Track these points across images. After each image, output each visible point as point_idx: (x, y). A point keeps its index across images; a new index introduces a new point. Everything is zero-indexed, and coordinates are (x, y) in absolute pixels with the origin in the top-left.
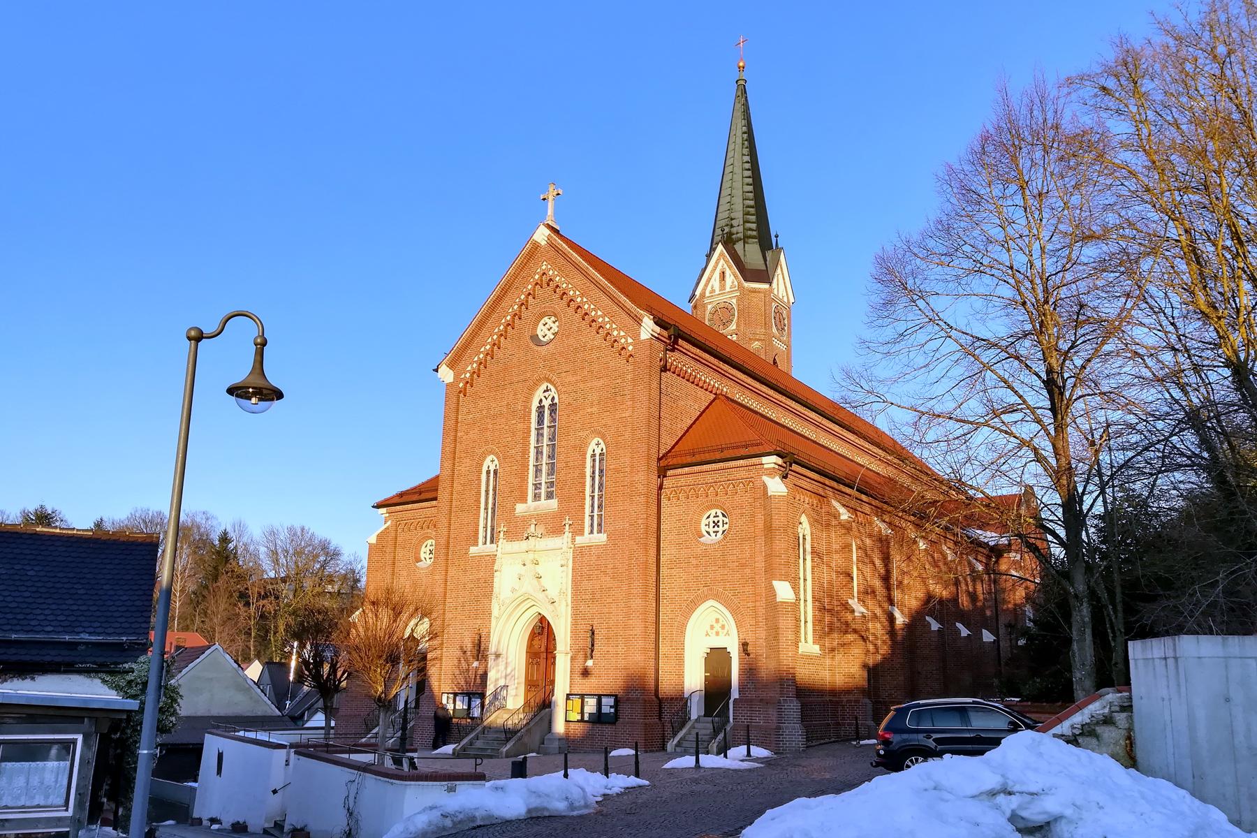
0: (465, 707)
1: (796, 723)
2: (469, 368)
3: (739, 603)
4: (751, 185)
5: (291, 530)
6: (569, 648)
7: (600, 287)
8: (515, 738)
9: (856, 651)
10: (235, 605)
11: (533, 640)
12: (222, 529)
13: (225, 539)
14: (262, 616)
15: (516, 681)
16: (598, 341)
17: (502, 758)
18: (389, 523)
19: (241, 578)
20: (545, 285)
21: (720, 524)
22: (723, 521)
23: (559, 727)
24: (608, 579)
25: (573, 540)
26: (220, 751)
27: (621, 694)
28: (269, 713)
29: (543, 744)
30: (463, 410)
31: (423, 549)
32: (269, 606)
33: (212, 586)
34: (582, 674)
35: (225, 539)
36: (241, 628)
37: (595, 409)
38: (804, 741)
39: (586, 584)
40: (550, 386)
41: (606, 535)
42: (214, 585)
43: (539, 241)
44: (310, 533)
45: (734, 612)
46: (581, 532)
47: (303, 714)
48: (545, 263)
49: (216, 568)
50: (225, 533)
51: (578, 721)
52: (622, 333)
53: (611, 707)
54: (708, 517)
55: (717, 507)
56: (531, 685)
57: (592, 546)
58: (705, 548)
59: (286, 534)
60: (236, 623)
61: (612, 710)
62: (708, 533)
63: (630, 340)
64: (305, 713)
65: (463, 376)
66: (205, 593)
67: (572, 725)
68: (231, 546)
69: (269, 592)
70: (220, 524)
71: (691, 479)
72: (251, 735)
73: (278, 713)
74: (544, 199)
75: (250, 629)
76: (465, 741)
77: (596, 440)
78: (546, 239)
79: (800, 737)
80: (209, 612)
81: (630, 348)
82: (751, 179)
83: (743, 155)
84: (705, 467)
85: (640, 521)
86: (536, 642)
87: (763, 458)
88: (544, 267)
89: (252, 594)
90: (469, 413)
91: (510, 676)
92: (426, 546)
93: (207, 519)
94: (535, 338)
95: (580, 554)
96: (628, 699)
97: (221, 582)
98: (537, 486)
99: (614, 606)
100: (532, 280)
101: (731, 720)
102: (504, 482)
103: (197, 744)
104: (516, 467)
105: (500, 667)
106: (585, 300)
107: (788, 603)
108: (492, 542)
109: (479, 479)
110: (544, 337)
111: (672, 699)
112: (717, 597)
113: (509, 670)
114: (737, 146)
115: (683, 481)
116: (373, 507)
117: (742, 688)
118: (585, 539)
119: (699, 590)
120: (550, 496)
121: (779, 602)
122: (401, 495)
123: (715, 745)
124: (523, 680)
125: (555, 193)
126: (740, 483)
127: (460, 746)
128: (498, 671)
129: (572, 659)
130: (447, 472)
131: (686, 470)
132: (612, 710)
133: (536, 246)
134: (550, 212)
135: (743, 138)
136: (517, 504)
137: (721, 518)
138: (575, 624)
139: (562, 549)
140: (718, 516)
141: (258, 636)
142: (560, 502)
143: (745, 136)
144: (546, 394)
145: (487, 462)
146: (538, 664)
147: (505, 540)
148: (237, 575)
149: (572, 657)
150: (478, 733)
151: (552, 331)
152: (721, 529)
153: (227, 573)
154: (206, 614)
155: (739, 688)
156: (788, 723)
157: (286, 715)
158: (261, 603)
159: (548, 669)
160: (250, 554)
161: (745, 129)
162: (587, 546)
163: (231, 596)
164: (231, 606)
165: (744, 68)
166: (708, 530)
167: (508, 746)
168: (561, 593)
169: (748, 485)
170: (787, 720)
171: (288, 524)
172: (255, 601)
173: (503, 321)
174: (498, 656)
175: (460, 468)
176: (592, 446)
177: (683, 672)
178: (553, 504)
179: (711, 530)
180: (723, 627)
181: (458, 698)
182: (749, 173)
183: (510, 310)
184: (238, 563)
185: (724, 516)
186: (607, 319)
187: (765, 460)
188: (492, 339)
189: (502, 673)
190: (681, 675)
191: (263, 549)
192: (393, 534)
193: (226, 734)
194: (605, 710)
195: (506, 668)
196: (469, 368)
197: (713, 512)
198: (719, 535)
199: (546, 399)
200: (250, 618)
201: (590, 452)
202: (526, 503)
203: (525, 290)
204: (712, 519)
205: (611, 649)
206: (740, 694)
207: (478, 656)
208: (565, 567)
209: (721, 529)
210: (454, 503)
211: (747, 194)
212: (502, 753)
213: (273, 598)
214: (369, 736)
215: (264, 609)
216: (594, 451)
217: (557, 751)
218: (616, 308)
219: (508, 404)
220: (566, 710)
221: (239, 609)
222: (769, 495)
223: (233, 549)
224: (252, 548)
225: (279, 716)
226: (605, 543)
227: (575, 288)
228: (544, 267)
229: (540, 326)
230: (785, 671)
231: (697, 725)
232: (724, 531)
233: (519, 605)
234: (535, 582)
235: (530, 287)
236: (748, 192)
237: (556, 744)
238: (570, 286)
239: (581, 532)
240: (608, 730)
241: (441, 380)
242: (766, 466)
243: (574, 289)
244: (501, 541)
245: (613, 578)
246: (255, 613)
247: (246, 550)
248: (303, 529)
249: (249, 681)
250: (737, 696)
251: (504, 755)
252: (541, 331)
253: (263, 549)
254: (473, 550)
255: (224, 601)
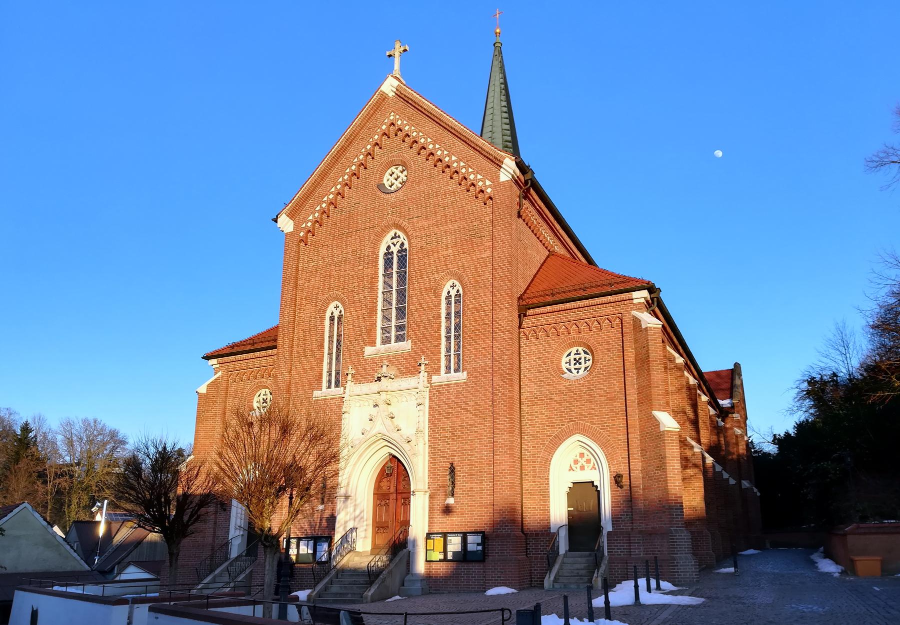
0: (310, 551)
1: (687, 553)
2: (311, 218)
3: (609, 436)
4: (508, 124)
5: (85, 421)
6: (427, 487)
7: (454, 132)
8: (378, 581)
9: (697, 485)
10: (35, 483)
11: (380, 482)
12: (24, 421)
13: (26, 429)
14: (59, 492)
15: (365, 523)
16: (453, 185)
17: (367, 602)
18: (220, 374)
19: (40, 461)
20: (392, 135)
21: (582, 361)
22: (570, 365)
23: (420, 567)
24: (470, 416)
25: (429, 380)
26: (35, 609)
27: (488, 530)
28: (78, 568)
29: (403, 585)
30: (304, 258)
31: (256, 399)
32: (64, 483)
33: (14, 468)
34: (442, 512)
35: (26, 429)
36: (39, 502)
37: (450, 252)
38: (697, 572)
39: (447, 423)
40: (399, 233)
41: (465, 373)
42: (16, 467)
43: (387, 93)
44: (102, 424)
45: (603, 445)
46: (438, 372)
47: (113, 569)
48: (393, 114)
49: (17, 453)
50: (27, 424)
51: (440, 561)
52: (479, 177)
53: (478, 544)
54: (569, 355)
55: (579, 344)
56: (379, 527)
57: (451, 384)
58: (568, 384)
59: (81, 424)
60: (34, 499)
61: (480, 548)
62: (569, 370)
63: (488, 183)
64: (115, 567)
65: (304, 225)
66: (8, 473)
67: (434, 565)
68: (31, 435)
69: (65, 472)
70: (21, 418)
71: (551, 318)
72: (71, 590)
73: (87, 567)
74: (390, 56)
75: (47, 503)
76: (319, 587)
77: (450, 283)
78: (395, 90)
79: (693, 567)
80: (11, 489)
81: (489, 190)
82: (508, 120)
83: (501, 100)
84: (569, 305)
85: (505, 357)
86: (385, 484)
87: (633, 293)
88: (392, 118)
89: (50, 473)
90: (311, 261)
91: (359, 518)
92: (259, 396)
93: (10, 414)
94: (381, 187)
95: (437, 392)
96: (498, 536)
97: (21, 465)
98: (386, 330)
99: (477, 443)
100: (379, 130)
101: (606, 553)
102: (351, 327)
103: (6, 601)
104: (363, 311)
105: (349, 510)
106: (437, 146)
107: (672, 432)
108: (337, 385)
109: (323, 326)
110: (391, 187)
111: (537, 534)
112: (584, 431)
113: (357, 513)
114: (495, 93)
115: (543, 319)
116: (203, 358)
117: (615, 519)
118: (442, 378)
119: (563, 425)
120: (399, 339)
121: (663, 431)
122: (233, 346)
123: (600, 579)
124: (370, 522)
125: (402, 49)
126: (605, 320)
127: (315, 593)
128: (347, 514)
129: (431, 497)
130: (288, 319)
131: (548, 308)
132: (480, 548)
133: (384, 97)
134: (397, 66)
135: (501, 87)
136: (366, 347)
137: (583, 355)
138: (433, 461)
139: (418, 388)
140: (580, 354)
141: (53, 508)
142: (414, 344)
143: (503, 86)
144: (395, 241)
145: (331, 308)
146: (387, 505)
147: (353, 383)
148: (36, 459)
149: (430, 496)
150: (331, 577)
151: (400, 180)
152: (583, 366)
153: (27, 457)
154: (7, 490)
155: (612, 521)
156: (680, 554)
157: (95, 570)
158: (58, 481)
159: (398, 510)
160: (49, 441)
161: (502, 80)
162: (445, 385)
163: (30, 476)
164: (31, 484)
165: (499, 34)
166: (569, 367)
167: (373, 590)
168: (418, 431)
169: (614, 321)
170: (679, 551)
171: (82, 416)
172: (52, 479)
173: (348, 170)
174: (347, 497)
175: (301, 315)
176: (447, 288)
177: (549, 507)
178: (406, 346)
179: (572, 367)
180: (588, 461)
181: (302, 543)
182: (506, 115)
183: (356, 160)
184: (38, 449)
185: (585, 353)
186: (462, 164)
187: (635, 294)
188: (336, 188)
189: (351, 515)
190: (547, 511)
191: (60, 438)
192: (224, 385)
193: (42, 589)
194: (471, 547)
195: (355, 510)
196: (311, 218)
197: (574, 350)
198: (581, 371)
199: (395, 245)
200: (47, 494)
201: (444, 294)
202: (375, 346)
203: (371, 140)
204: (572, 357)
205: (474, 486)
206: (613, 527)
207: (323, 499)
208: (421, 407)
209: (583, 366)
210: (295, 349)
211: (505, 131)
212: (366, 598)
213: (68, 477)
214: (200, 586)
215: (60, 486)
216: (449, 292)
217: (420, 593)
218: (472, 152)
219: (354, 251)
220: (427, 550)
221: (38, 486)
222: (643, 327)
223: (33, 438)
224: (50, 437)
225: (88, 571)
226: (465, 381)
227: (426, 135)
228: (392, 118)
229: (387, 175)
230: (673, 500)
231: (566, 560)
232: (586, 368)
233: (370, 446)
234: (389, 421)
235: (376, 137)
236: (506, 130)
237: (418, 586)
238: (421, 134)
239: (438, 372)
240: (475, 568)
241: (281, 229)
242: (635, 301)
243: (426, 136)
244: (349, 383)
245: (476, 415)
246: (51, 489)
247: (45, 438)
248: (95, 421)
249: (58, 538)
250: (610, 528)
251: (369, 599)
252: (387, 180)
253: (60, 438)
254: (317, 393)
255: (24, 480)
